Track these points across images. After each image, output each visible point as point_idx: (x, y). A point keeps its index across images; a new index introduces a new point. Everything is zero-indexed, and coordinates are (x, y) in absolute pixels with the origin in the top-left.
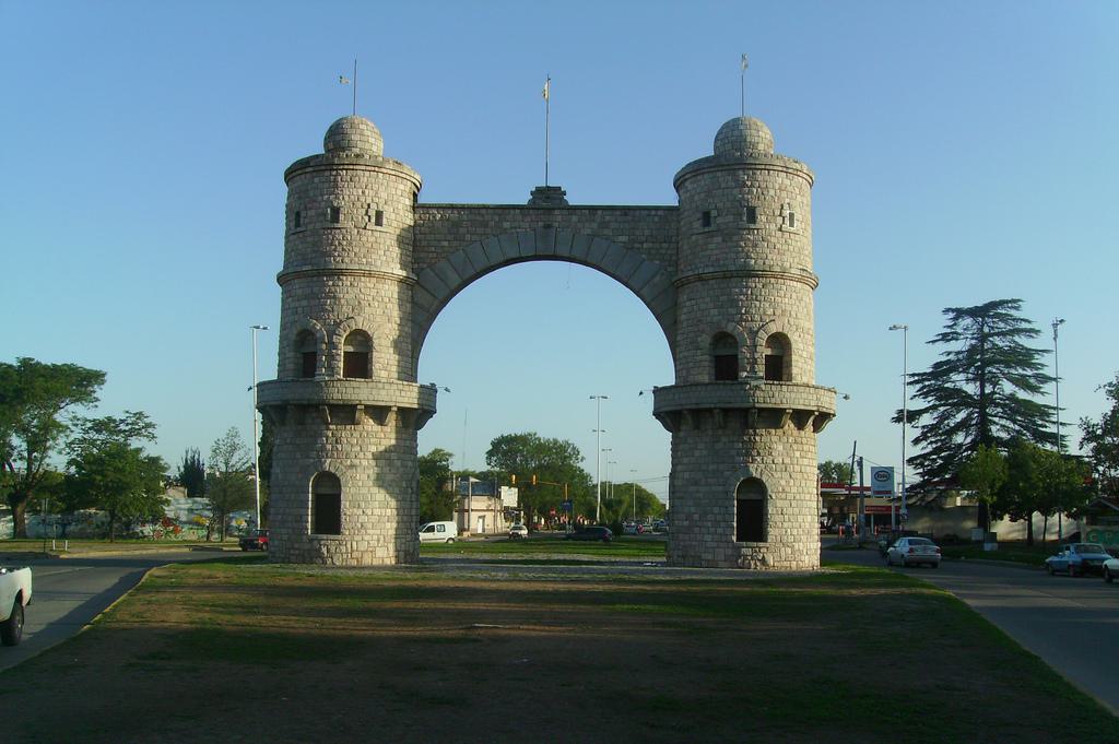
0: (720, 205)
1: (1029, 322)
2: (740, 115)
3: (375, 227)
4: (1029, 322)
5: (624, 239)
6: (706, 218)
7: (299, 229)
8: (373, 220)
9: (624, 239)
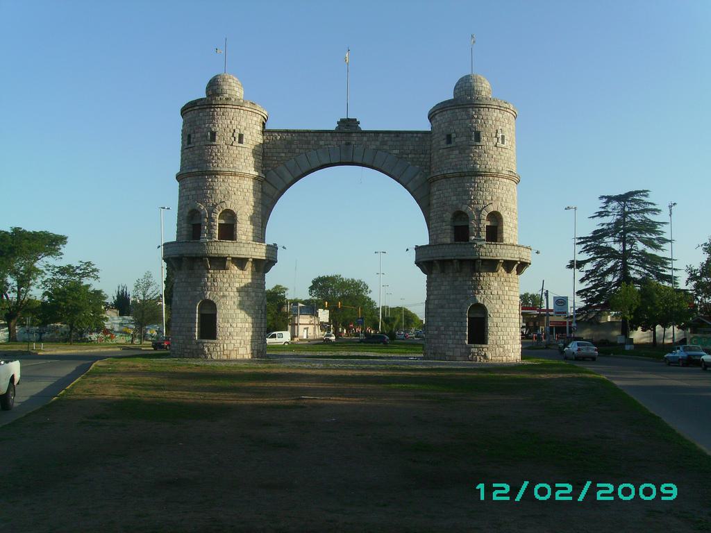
0: (457, 130)
1: (654, 205)
2: (470, 73)
3: (238, 145)
4: (654, 205)
5: (396, 152)
6: (449, 139)
7: (190, 146)
8: (237, 140)
9: (396, 152)
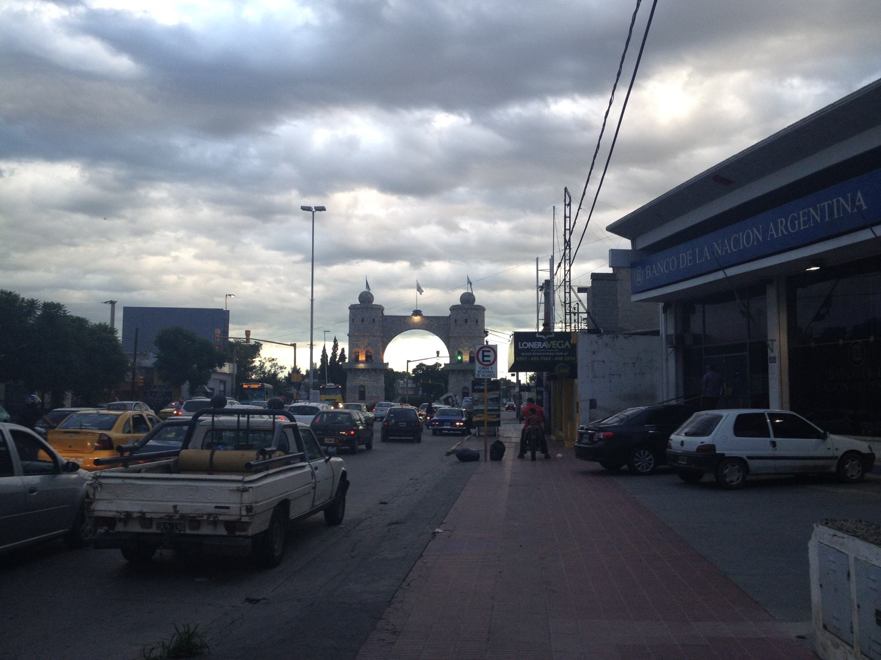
6: (456, 321)
